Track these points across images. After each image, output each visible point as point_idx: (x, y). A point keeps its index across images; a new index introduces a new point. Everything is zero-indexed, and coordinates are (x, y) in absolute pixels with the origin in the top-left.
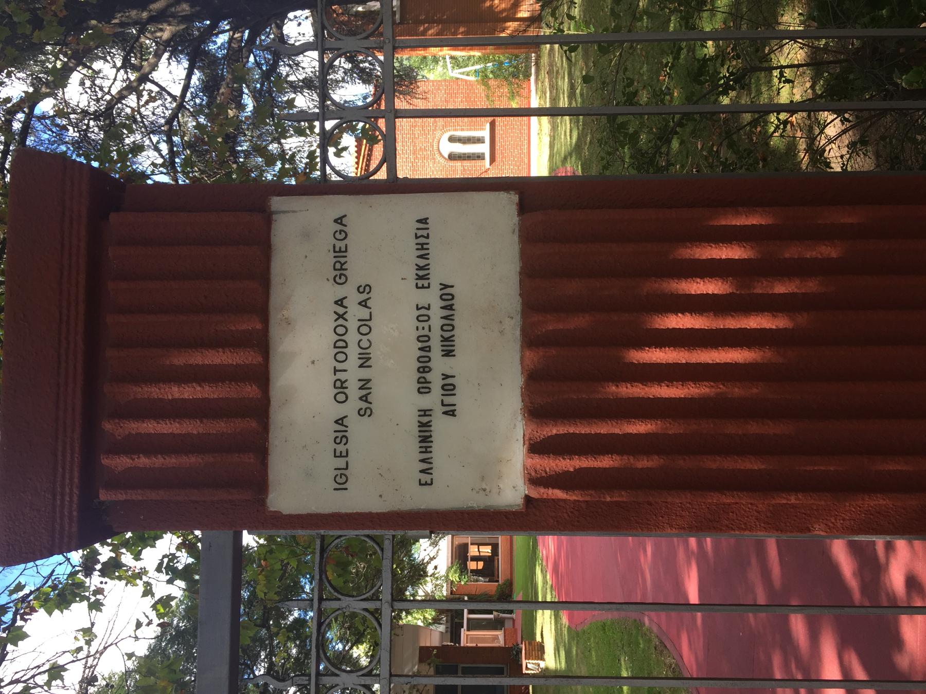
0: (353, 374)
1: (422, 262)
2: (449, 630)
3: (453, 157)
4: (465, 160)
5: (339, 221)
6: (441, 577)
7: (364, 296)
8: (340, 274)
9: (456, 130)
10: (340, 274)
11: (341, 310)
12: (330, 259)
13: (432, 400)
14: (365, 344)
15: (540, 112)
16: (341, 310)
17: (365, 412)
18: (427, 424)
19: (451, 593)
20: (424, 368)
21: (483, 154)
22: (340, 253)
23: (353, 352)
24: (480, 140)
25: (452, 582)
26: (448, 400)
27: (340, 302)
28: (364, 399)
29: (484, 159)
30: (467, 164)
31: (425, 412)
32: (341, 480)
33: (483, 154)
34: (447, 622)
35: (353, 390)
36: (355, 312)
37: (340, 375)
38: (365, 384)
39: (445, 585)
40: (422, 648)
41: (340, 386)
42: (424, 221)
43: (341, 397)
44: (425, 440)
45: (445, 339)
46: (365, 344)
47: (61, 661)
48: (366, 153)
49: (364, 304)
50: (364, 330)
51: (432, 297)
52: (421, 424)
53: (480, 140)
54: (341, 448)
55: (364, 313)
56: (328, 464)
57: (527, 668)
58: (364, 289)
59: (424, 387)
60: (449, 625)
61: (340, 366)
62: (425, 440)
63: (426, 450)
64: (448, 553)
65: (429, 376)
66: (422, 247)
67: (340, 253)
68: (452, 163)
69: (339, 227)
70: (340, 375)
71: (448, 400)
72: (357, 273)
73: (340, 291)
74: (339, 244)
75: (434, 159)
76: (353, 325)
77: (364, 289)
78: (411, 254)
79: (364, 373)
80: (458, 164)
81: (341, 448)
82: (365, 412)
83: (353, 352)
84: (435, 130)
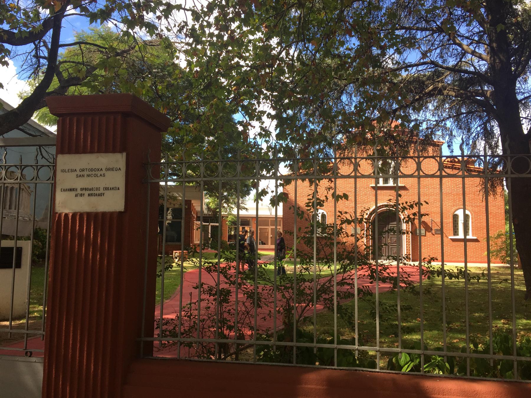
0: (86, 173)
1: (109, 189)
2: (205, 216)
3: (455, 217)
4: (454, 224)
5: (120, 169)
6: (231, 211)
7: (102, 175)
8: (108, 169)
9: (472, 219)
10: (108, 169)
11: (100, 170)
12: (111, 167)
13: (79, 192)
14: (92, 176)
15: (489, 266)
16: (100, 170)
17: (77, 176)
18: (74, 190)
19: (223, 217)
20: (86, 189)
21: (458, 235)
22: (112, 169)
23: (90, 173)
24: (466, 232)
25: (228, 217)
26: (79, 195)
27: (101, 170)
28: (80, 176)
29: (454, 235)
30: (451, 225)
31: (76, 190)
32: (63, 171)
33: (458, 235)
34: (209, 215)
35: (82, 173)
36: (99, 173)
37: (85, 170)
38: (83, 176)
39: (226, 213)
40: (190, 201)
41: (83, 170)
42: (119, 189)
43: (81, 170)
44: (71, 190)
45: (92, 194)
46: (92, 176)
47: (160, 21)
48: (457, 166)
49: (101, 175)
50: (95, 175)
51: (102, 191)
52: (74, 189)
53: (466, 232)
54: (70, 170)
55: (99, 175)
56: (66, 168)
57: (175, 253)
58: (104, 175)
59: (82, 189)
60: (208, 216)
61: (87, 170)
62: (71, 190)
63: (68, 190)
64: (263, 215)
65: (84, 190)
66: (113, 189)
67: (112, 169)
68: (451, 217)
69: (118, 169)
70: (85, 170)
71: (79, 195)
72: (108, 174)
73: (104, 170)
74: (114, 169)
75: (454, 206)
76: (96, 173)
77: (104, 175)
78: (112, 186)
79: (85, 176)
80: (451, 220)
81: (70, 170)
82: (77, 176)
83: (90, 173)
84: (472, 206)
